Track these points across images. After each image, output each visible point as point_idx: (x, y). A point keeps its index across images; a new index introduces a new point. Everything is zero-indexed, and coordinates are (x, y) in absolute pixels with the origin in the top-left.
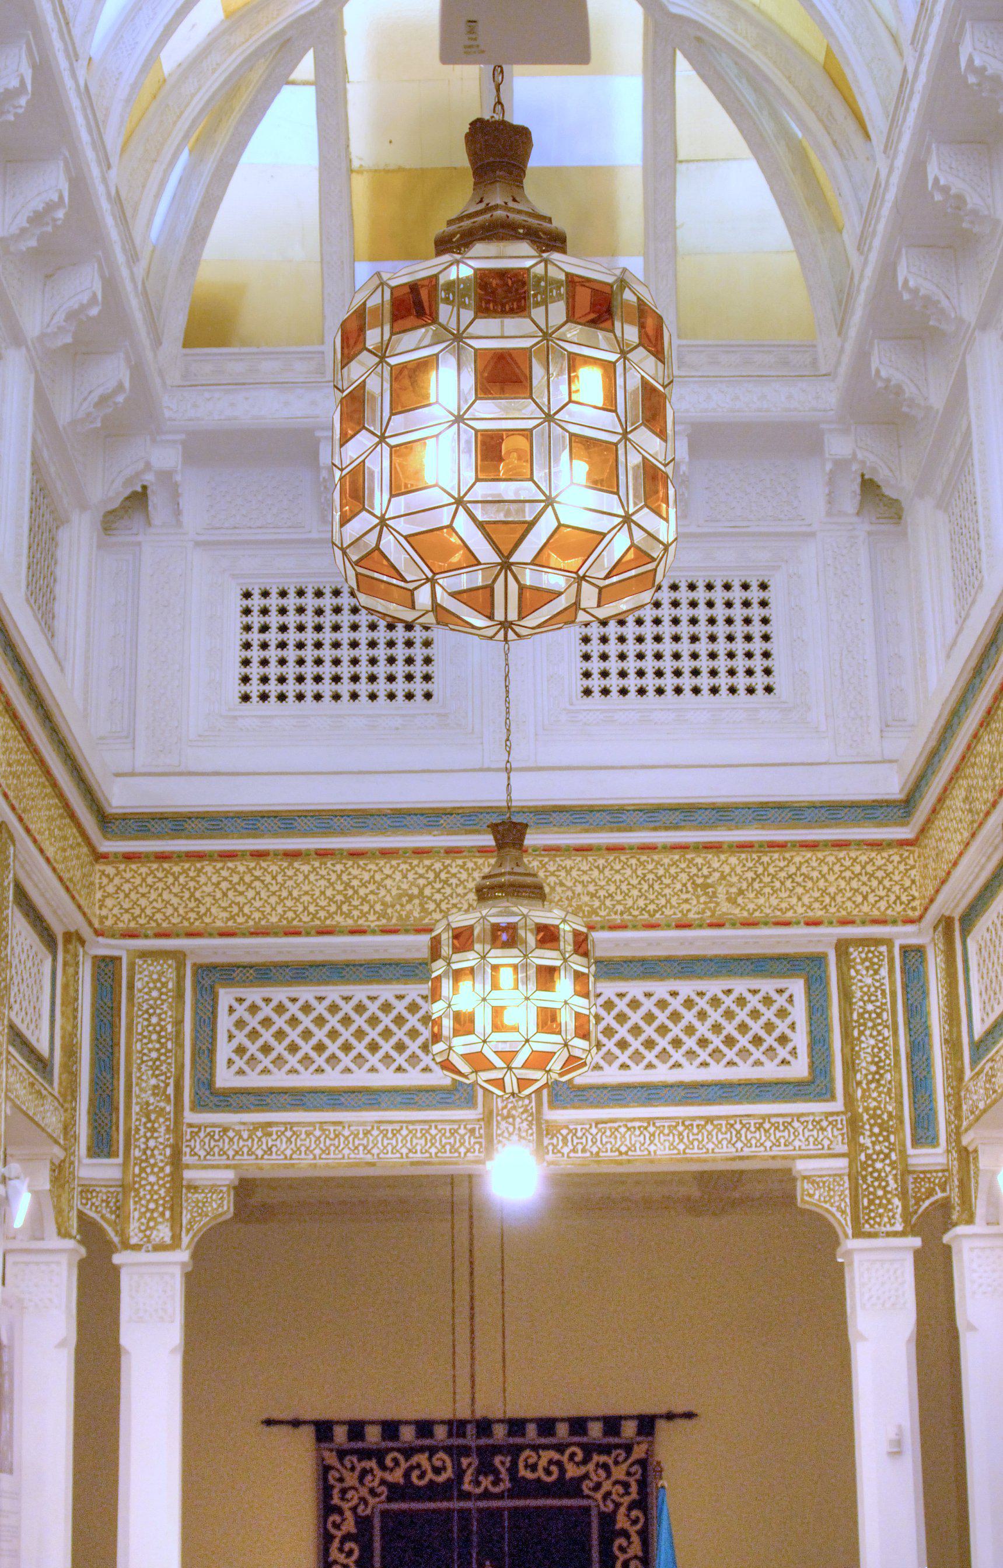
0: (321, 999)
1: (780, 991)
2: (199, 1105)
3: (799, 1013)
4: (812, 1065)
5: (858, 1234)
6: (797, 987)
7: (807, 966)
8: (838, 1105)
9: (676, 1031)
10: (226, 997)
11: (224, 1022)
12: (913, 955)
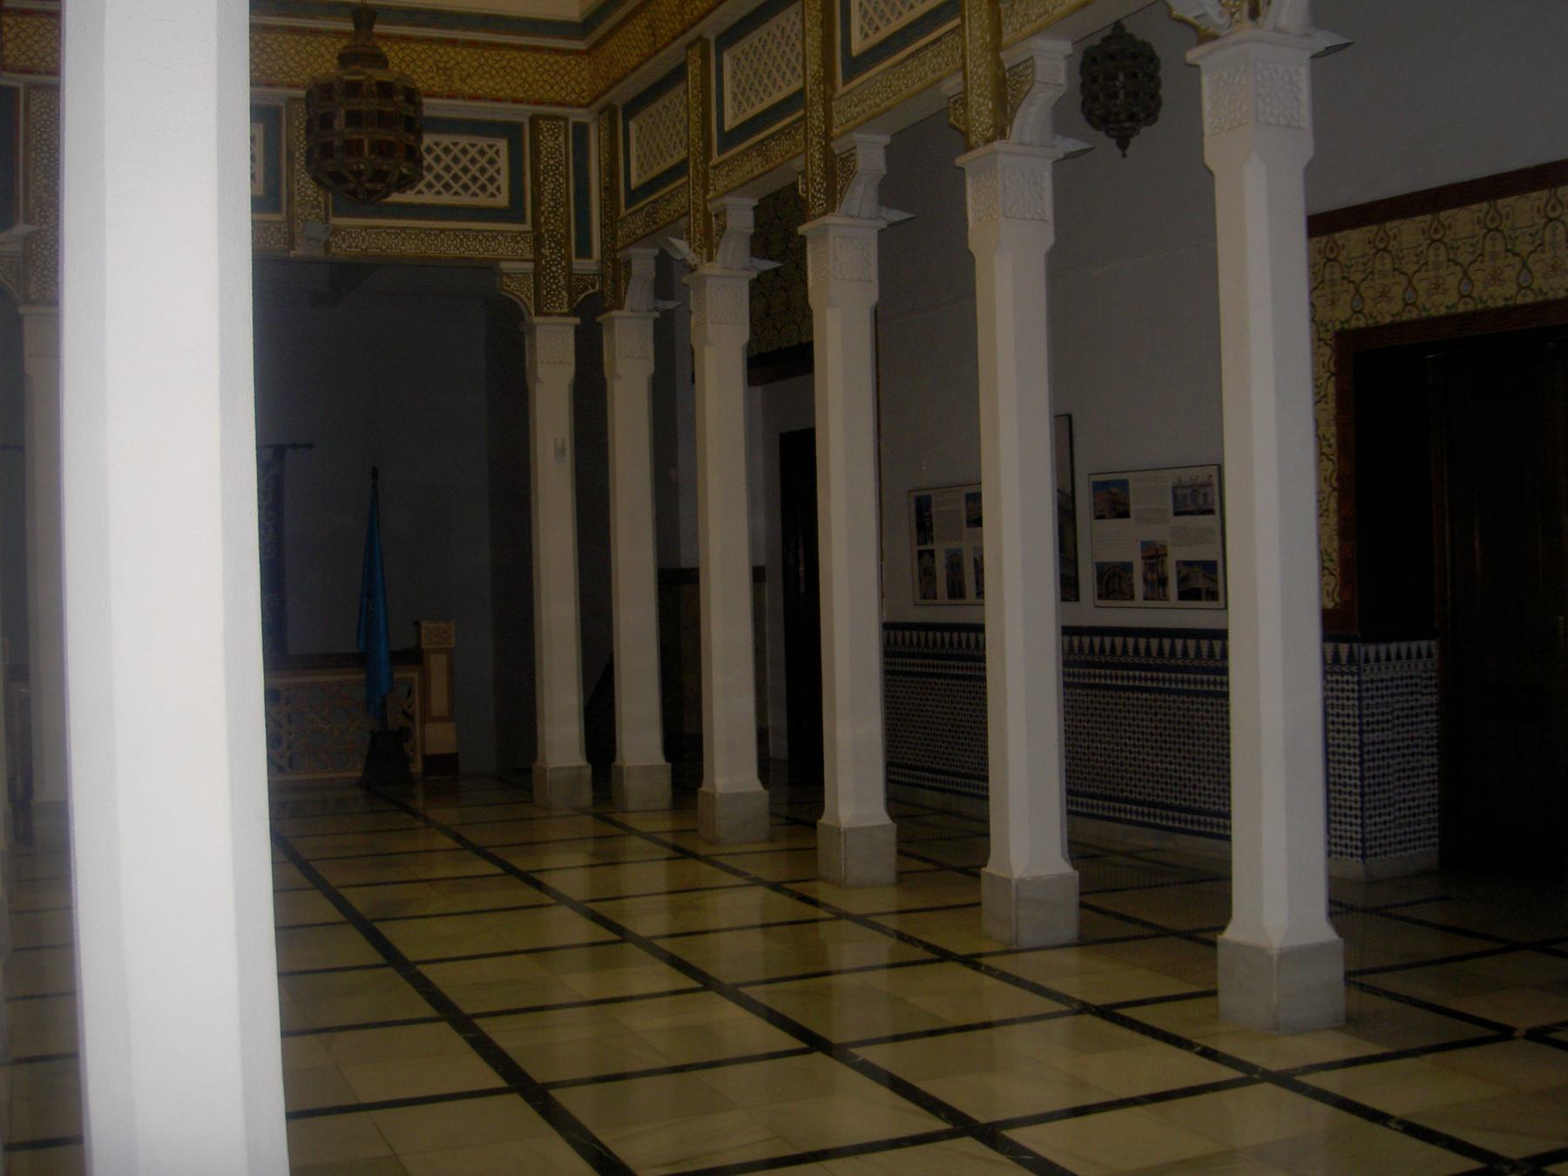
1: (491, 147)
3: (503, 162)
4: (511, 200)
5: (539, 313)
6: (502, 145)
7: (509, 131)
8: (528, 227)
9: (474, 170)
12: (581, 130)
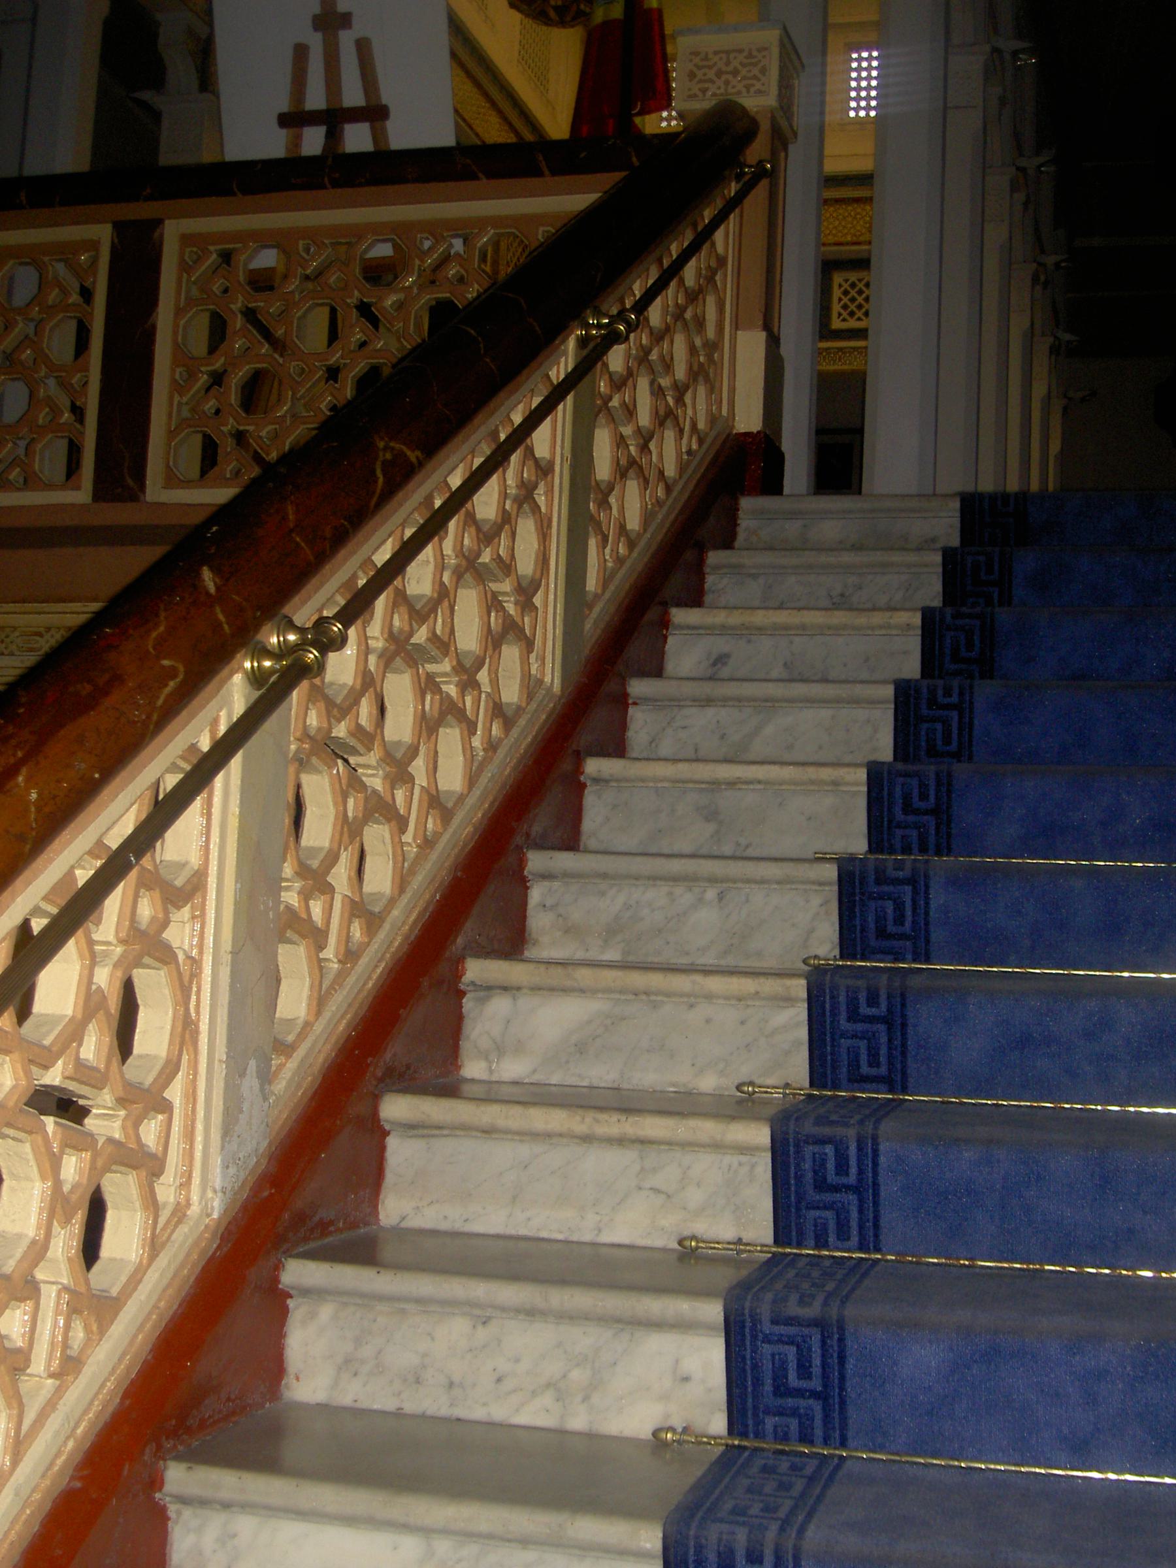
0: (860, 280)
2: (823, 337)
10: (838, 278)
11: (837, 293)
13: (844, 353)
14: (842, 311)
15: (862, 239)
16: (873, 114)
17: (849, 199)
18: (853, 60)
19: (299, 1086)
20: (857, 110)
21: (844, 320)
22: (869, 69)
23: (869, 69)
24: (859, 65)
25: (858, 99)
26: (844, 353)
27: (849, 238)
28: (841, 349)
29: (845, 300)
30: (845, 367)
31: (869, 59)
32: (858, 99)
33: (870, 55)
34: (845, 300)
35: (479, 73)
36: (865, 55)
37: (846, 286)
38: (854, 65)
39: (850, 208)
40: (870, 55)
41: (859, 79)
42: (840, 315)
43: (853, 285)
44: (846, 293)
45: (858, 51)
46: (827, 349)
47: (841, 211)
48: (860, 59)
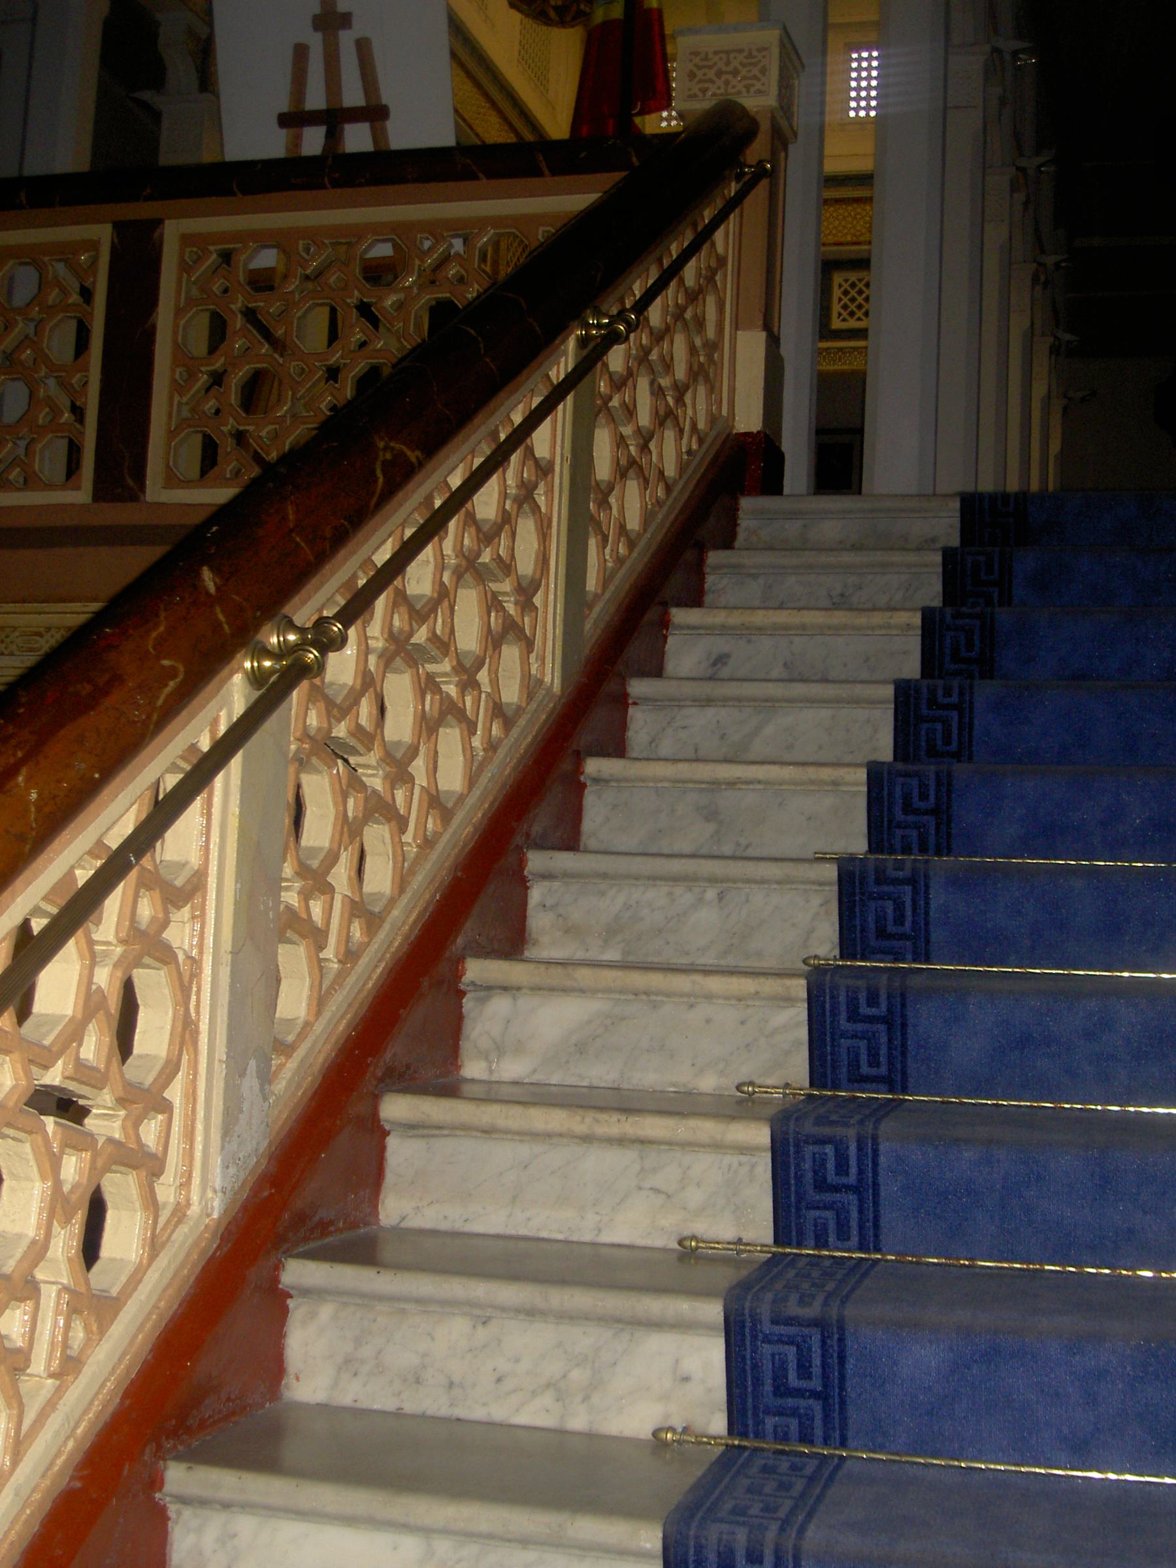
0: (860, 280)
2: (823, 337)
10: (838, 278)
11: (837, 293)
13: (844, 353)
14: (842, 311)
15: (862, 239)
16: (873, 114)
17: (849, 199)
18: (853, 60)
19: (299, 1086)
20: (857, 110)
21: (844, 320)
22: (869, 69)
23: (869, 69)
24: (859, 65)
25: (858, 99)
26: (844, 353)
27: (849, 238)
28: (841, 349)
29: (845, 300)
30: (845, 367)
31: (869, 59)
32: (858, 99)
33: (870, 55)
34: (845, 300)
35: (479, 73)
36: (865, 55)
37: (846, 286)
38: (854, 65)
39: (850, 208)
40: (870, 55)
41: (859, 79)
42: (840, 315)
43: (853, 285)
44: (846, 293)
45: (858, 51)
46: (827, 349)
47: (841, 211)
48: (860, 59)
